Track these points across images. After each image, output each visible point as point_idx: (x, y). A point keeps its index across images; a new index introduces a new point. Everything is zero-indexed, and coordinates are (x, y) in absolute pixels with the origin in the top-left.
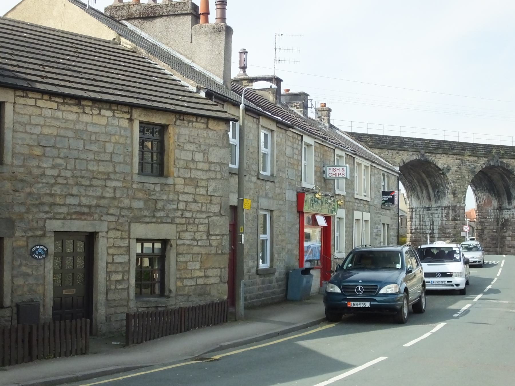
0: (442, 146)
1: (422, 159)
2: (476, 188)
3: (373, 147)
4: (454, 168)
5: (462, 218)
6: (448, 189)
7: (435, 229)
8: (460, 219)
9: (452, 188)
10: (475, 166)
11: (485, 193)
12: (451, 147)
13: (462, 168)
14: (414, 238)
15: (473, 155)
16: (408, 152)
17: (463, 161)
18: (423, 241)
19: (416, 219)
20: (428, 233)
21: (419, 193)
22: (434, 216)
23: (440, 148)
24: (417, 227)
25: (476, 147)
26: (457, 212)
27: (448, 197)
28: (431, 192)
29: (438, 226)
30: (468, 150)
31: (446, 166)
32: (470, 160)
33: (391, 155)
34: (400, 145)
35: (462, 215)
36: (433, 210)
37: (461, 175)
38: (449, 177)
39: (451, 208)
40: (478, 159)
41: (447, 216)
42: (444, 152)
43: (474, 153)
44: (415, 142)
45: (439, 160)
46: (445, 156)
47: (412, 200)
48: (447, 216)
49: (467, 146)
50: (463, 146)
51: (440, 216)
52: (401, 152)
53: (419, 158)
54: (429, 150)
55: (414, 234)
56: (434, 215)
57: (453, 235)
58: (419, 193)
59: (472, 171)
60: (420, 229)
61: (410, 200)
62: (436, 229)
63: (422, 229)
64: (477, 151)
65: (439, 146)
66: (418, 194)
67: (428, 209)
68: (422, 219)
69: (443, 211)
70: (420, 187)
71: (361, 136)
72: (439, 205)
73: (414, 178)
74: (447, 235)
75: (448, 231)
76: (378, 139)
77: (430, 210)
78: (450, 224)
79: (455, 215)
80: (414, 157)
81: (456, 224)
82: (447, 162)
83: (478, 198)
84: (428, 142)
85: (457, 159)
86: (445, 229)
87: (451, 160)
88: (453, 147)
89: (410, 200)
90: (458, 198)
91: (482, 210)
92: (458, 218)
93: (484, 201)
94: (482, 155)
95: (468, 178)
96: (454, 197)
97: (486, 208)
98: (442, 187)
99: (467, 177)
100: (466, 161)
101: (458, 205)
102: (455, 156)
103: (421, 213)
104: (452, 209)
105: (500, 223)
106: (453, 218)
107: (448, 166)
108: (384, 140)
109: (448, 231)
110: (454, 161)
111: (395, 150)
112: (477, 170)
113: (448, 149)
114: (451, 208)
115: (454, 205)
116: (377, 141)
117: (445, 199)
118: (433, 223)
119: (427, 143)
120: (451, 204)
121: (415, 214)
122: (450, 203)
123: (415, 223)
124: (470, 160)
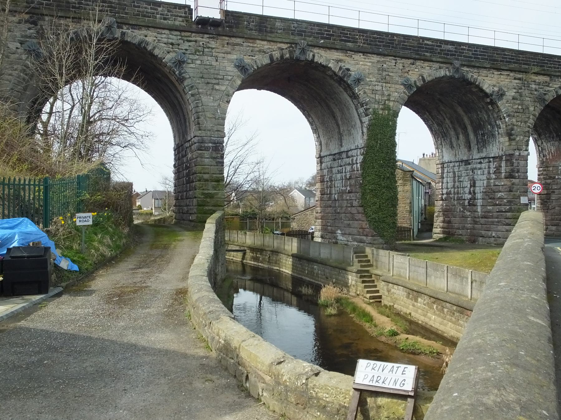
0: (490, 56)
1: (457, 76)
2: (539, 135)
3: (368, 51)
4: (511, 93)
5: (522, 175)
6: (500, 128)
7: (478, 193)
8: (519, 176)
9: (506, 126)
10: (545, 91)
11: (553, 142)
12: (506, 58)
13: (523, 93)
14: (445, 206)
15: (543, 72)
16: (431, 63)
17: (526, 82)
18: (458, 211)
19: (449, 179)
20: (466, 198)
21: (454, 140)
22: (476, 173)
23: (486, 59)
24: (450, 191)
25: (547, 60)
26: (515, 165)
27: (499, 141)
28: (472, 136)
29: (482, 188)
30: (534, 65)
31: (496, 89)
32: (537, 81)
33: (401, 67)
34: (418, 51)
35: (522, 170)
36: (474, 164)
37: (522, 105)
38: (501, 108)
39: (504, 159)
40: (551, 80)
41: (498, 168)
42: (493, 66)
43: (544, 70)
44: (444, 47)
45: (485, 78)
46: (496, 73)
47: (442, 152)
48: (498, 171)
49: (532, 59)
50: (526, 58)
51: (486, 172)
52: (418, 63)
53: (451, 74)
54: (469, 61)
55: (446, 200)
56: (475, 171)
57: (508, 202)
58: (454, 140)
59: (540, 99)
60: (454, 193)
61: (440, 151)
62: (479, 192)
63: (458, 193)
64: (550, 67)
65: (485, 55)
66: (451, 142)
67: (467, 162)
68: (457, 178)
69: (491, 164)
70: (455, 130)
71: (346, 32)
72: (483, 155)
73: (445, 116)
74: (497, 202)
75: (499, 195)
76: (378, 38)
77: (469, 164)
78: (503, 184)
79: (512, 170)
80: (442, 73)
81: (513, 184)
82: (498, 83)
83: (542, 150)
84: (467, 48)
85: (515, 79)
86: (494, 192)
87: (507, 80)
88: (509, 58)
89: (440, 151)
90: (517, 142)
91: (548, 167)
92: (517, 175)
93: (552, 153)
94: (558, 74)
95: (534, 110)
96: (510, 140)
97: (554, 163)
98: (489, 127)
99: (532, 109)
100: (530, 83)
101: (517, 153)
102: (512, 74)
103: (456, 169)
104: (506, 160)
105: (416, 209)
106: (508, 174)
107: (500, 89)
108: (389, 40)
109: (499, 195)
110: (511, 82)
111: (408, 58)
112: (549, 97)
113: (501, 61)
114: (504, 159)
115: (510, 153)
116: (376, 41)
117: (494, 145)
118: (474, 183)
119: (465, 49)
120: (505, 152)
121: (447, 172)
122: (502, 150)
123: (447, 185)
124: (537, 81)
